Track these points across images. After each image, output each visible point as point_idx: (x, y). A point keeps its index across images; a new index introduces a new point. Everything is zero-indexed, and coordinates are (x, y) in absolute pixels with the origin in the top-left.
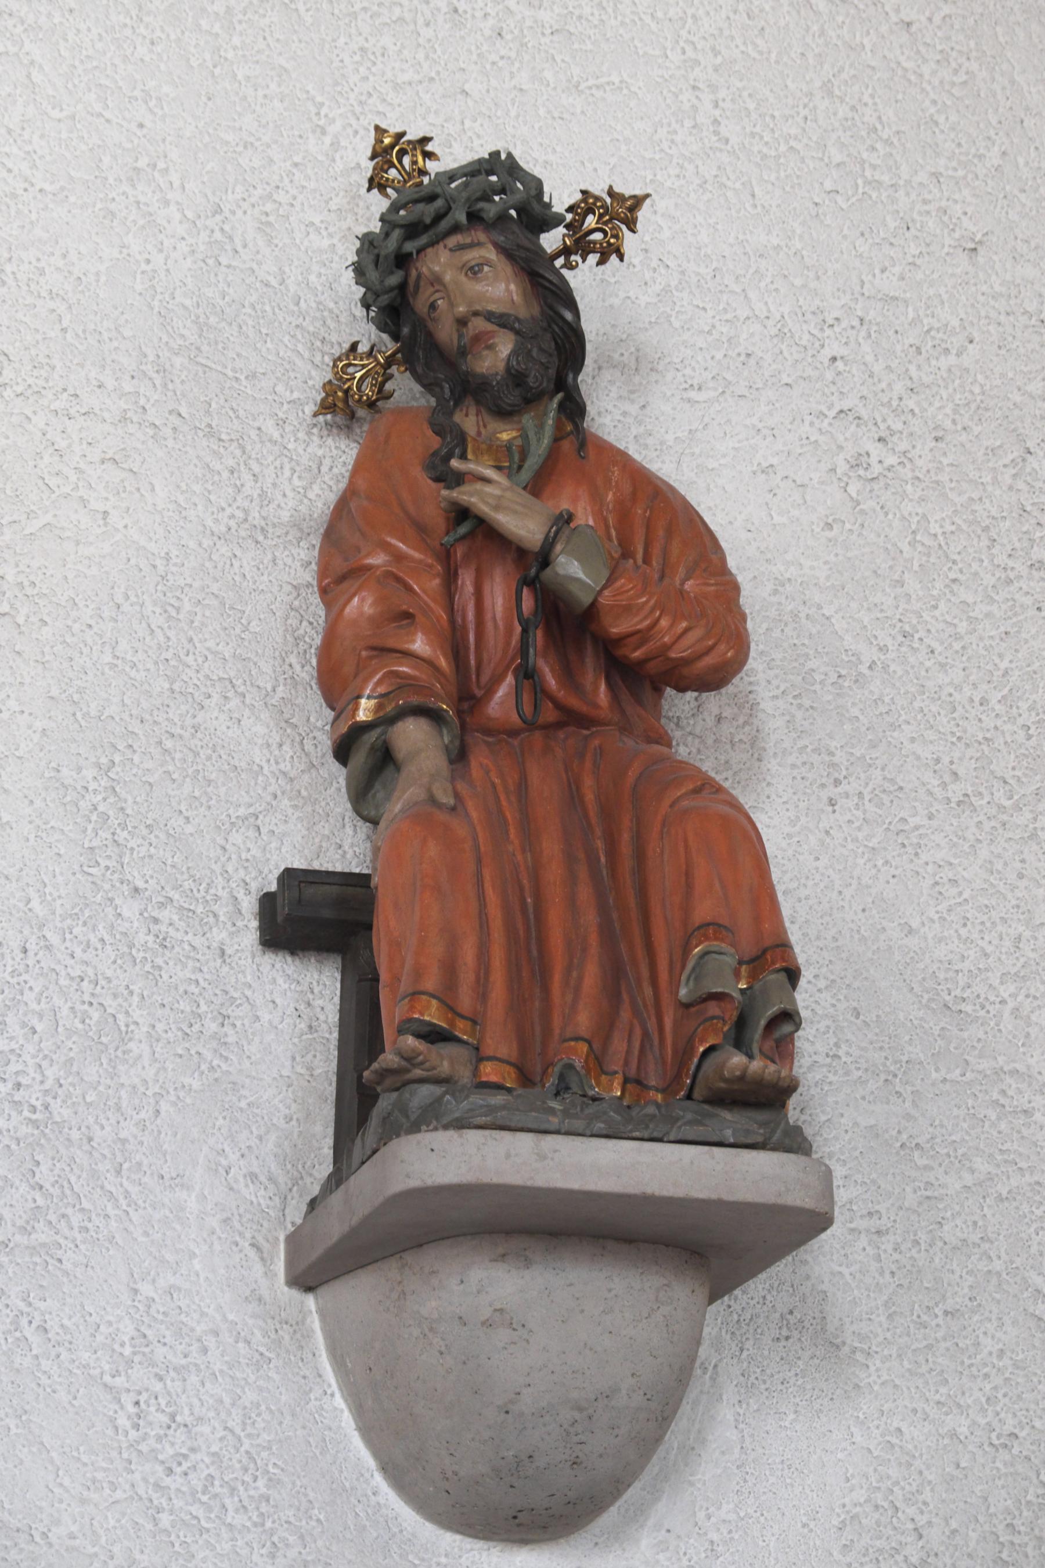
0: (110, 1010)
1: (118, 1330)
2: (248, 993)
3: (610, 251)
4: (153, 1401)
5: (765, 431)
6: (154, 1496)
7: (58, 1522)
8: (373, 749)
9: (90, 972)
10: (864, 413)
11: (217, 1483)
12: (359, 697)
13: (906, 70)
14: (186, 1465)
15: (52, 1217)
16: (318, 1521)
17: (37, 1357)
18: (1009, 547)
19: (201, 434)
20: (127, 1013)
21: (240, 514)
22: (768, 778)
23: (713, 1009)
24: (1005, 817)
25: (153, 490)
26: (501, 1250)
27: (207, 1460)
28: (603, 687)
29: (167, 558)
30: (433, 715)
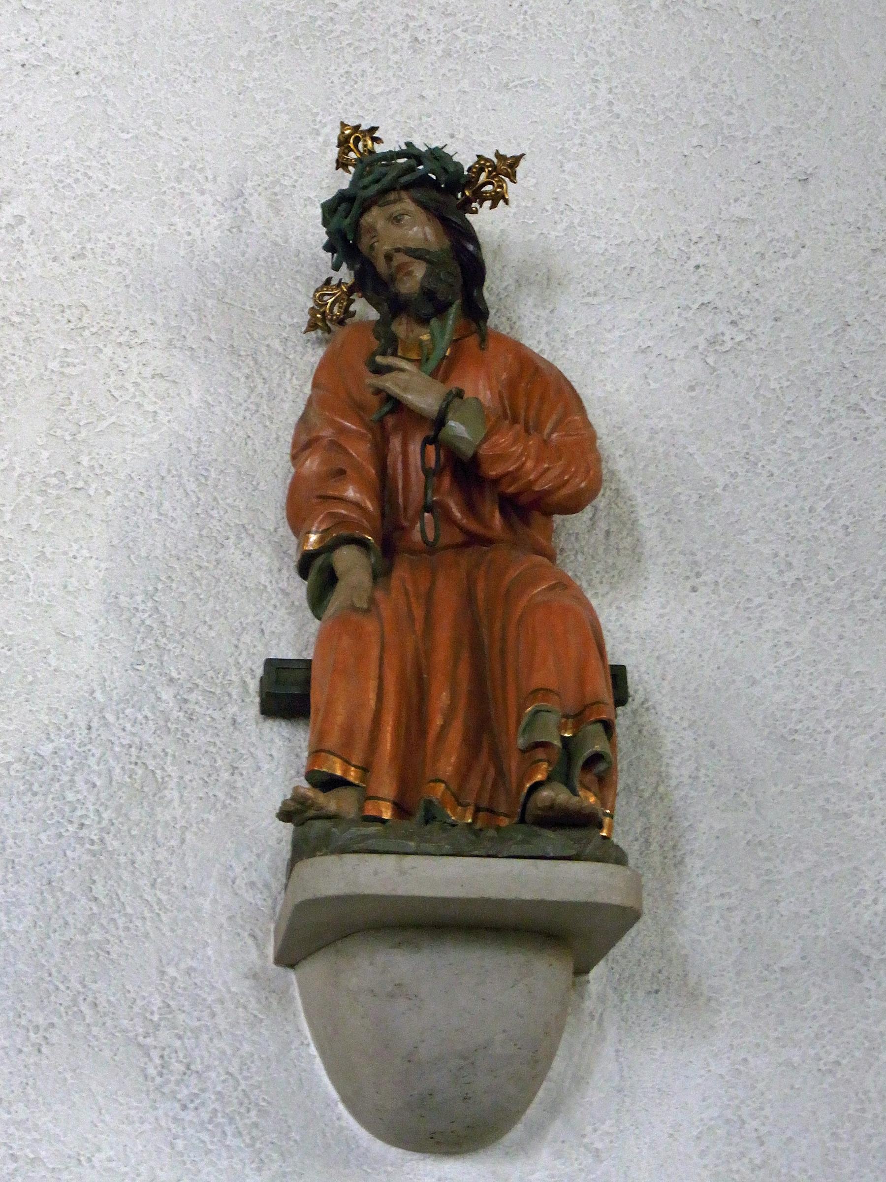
0: (151, 768)
1: (149, 1002)
2: (252, 750)
3: (498, 198)
4: (174, 1055)
5: (644, 323)
6: (172, 1126)
7: (99, 1150)
8: (321, 570)
9: (137, 740)
10: (719, 304)
11: (219, 1115)
12: (309, 532)
13: (754, 54)
14: (197, 1102)
15: (104, 922)
16: (295, 1141)
17: (88, 1025)
18: (832, 395)
19: (225, 352)
20: (163, 769)
21: (253, 407)
22: (646, 574)
23: (540, 754)
24: (828, 594)
25: (190, 394)
26: (397, 940)
27: (213, 1097)
28: (497, 515)
29: (199, 441)
30: (361, 543)
